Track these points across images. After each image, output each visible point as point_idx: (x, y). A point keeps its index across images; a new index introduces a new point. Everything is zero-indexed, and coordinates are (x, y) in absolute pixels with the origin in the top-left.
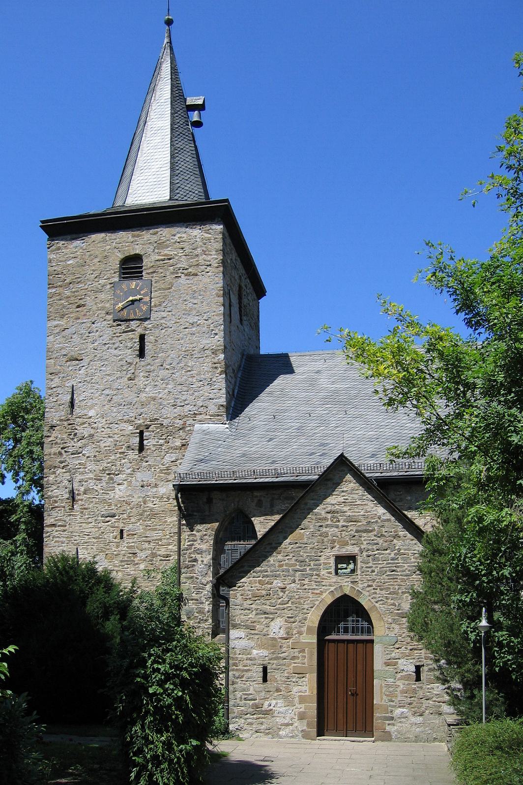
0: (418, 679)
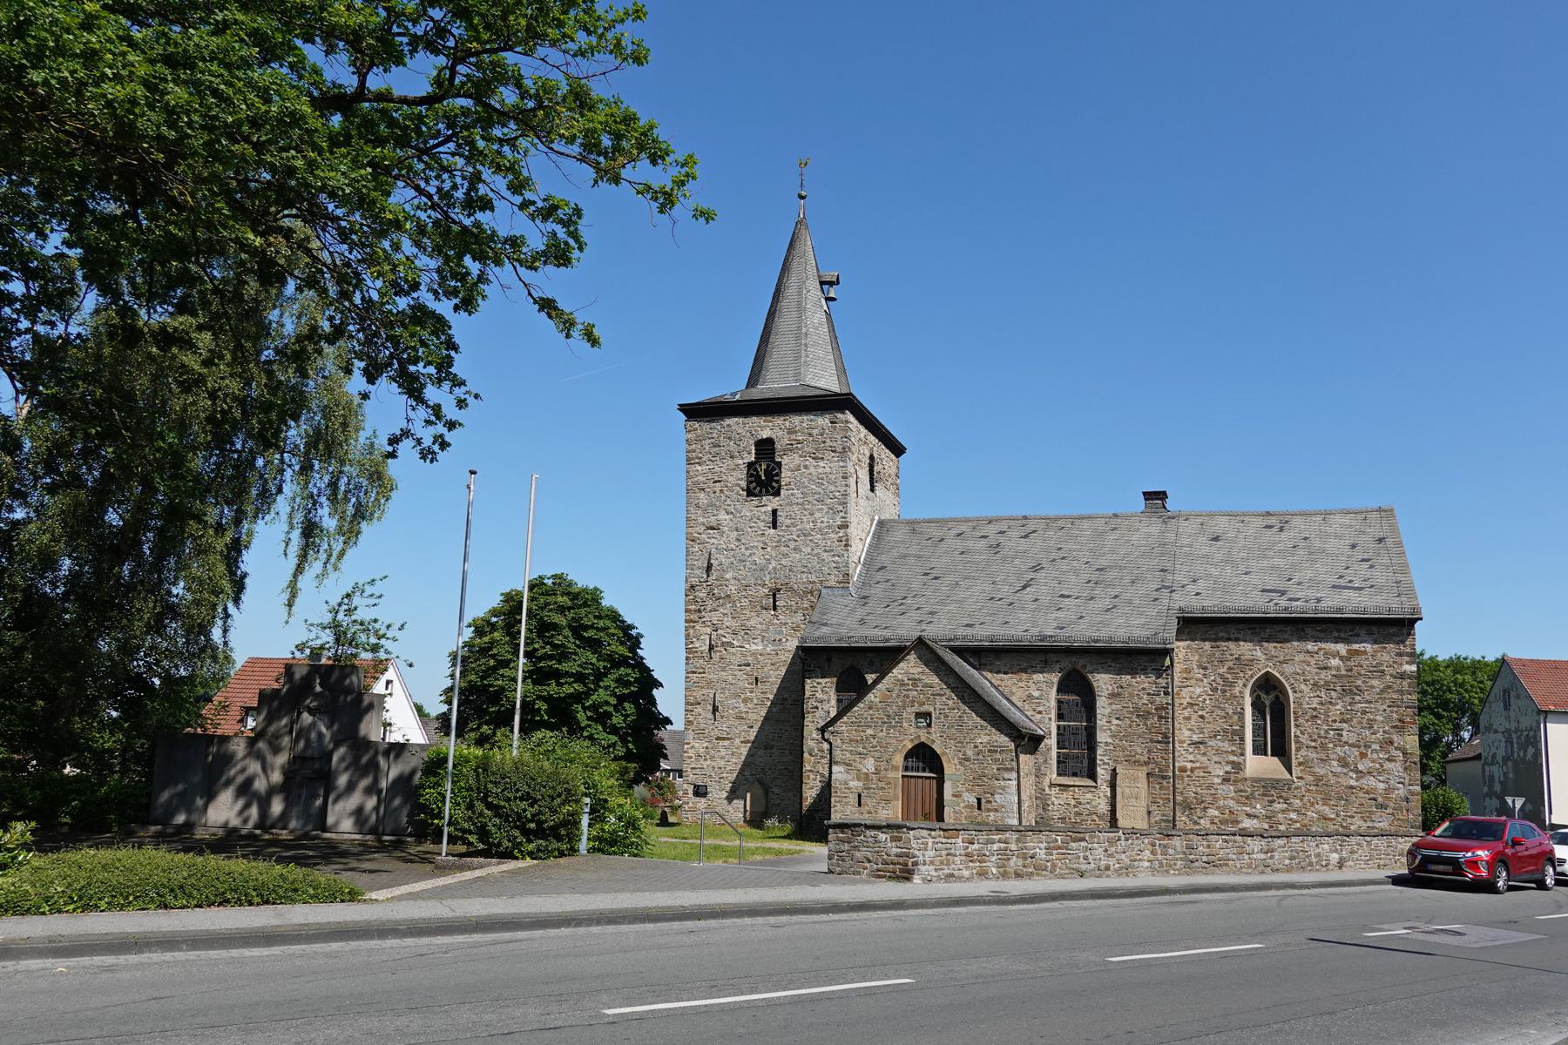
0: (979, 808)
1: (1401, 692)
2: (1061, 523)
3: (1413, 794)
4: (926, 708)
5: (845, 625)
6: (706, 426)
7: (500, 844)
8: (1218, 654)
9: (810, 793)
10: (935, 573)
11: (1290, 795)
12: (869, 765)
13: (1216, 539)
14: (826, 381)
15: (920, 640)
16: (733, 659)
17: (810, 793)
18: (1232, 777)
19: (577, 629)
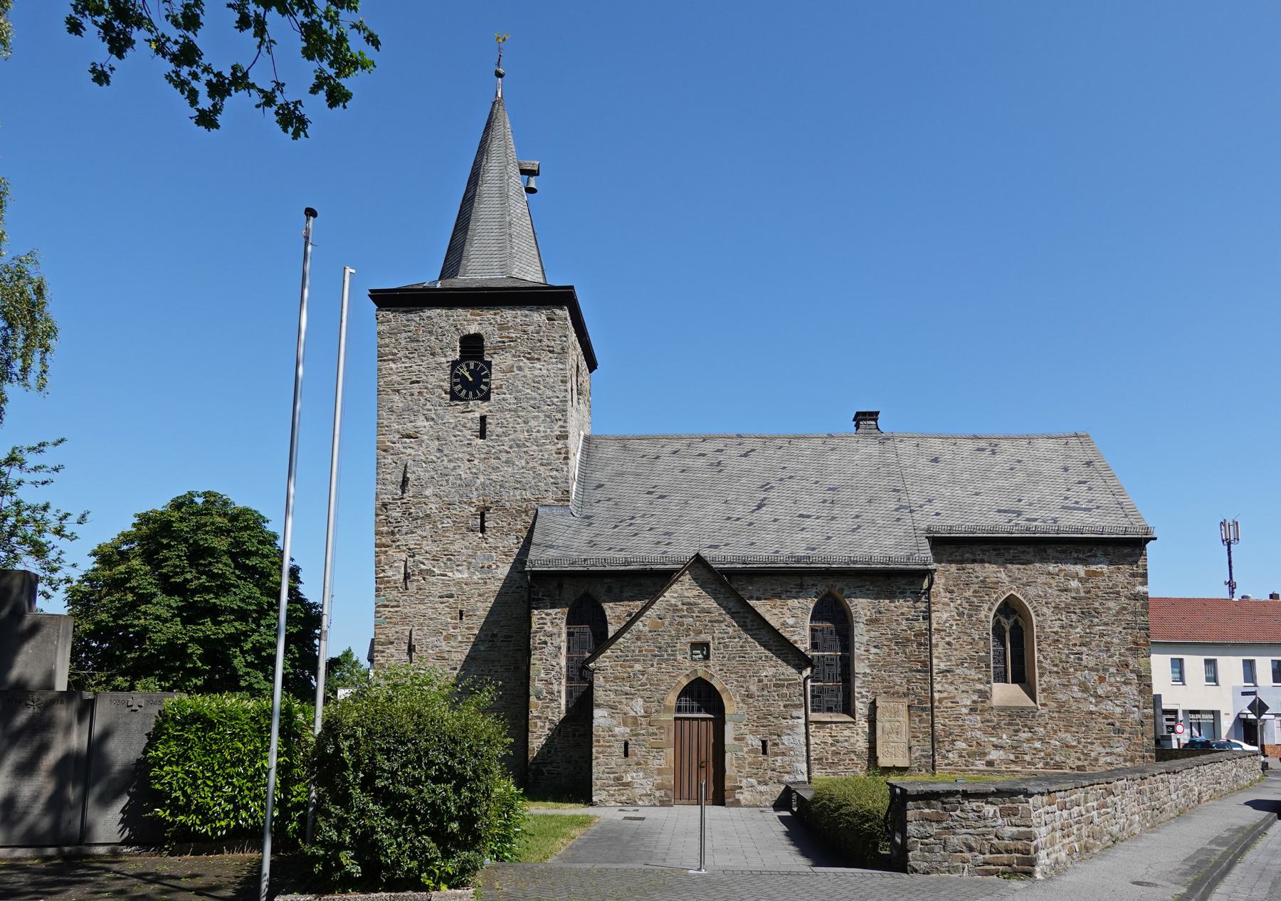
0: (765, 752)
1: (1134, 613)
2: (779, 442)
3: (1147, 717)
5: (564, 546)
6: (402, 318)
7: (397, 863)
8: (964, 577)
10: (659, 492)
11: (1035, 723)
12: (638, 706)
13: (936, 460)
14: (530, 274)
15: (698, 559)
16: (433, 589)
18: (979, 706)
19: (238, 554)
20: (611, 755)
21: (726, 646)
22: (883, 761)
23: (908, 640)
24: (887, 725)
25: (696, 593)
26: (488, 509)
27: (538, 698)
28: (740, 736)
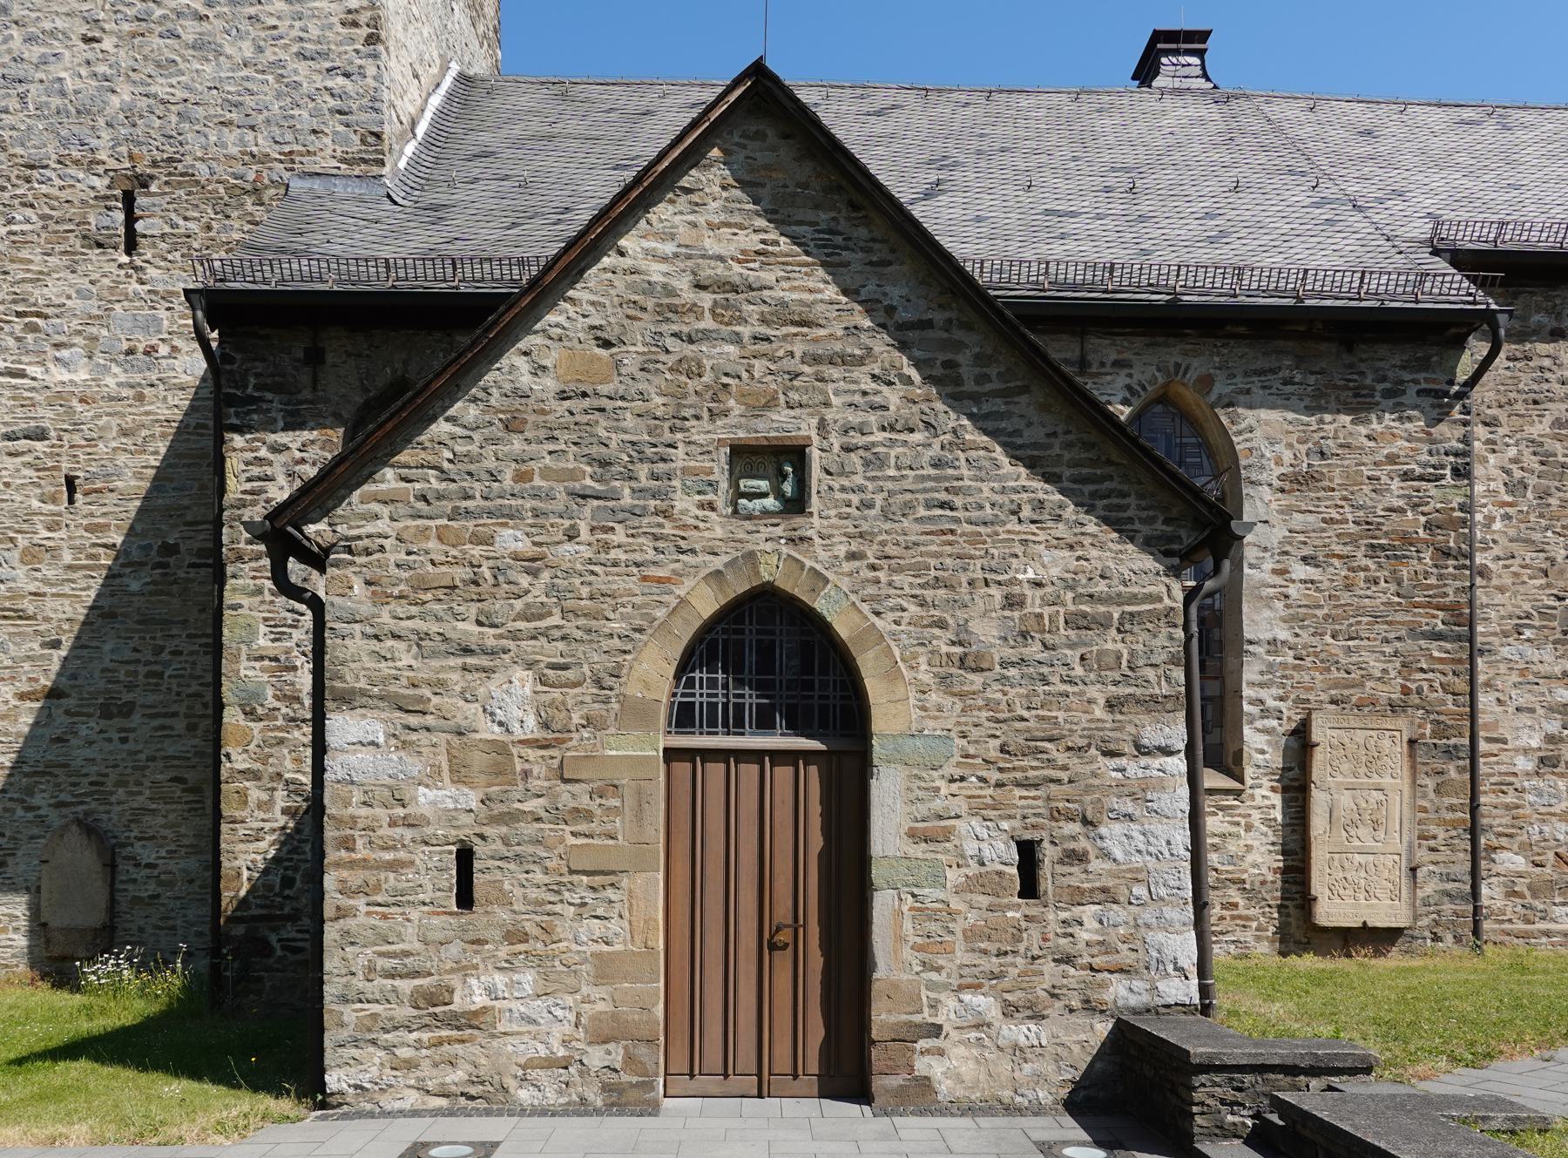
0: (1029, 888)
4: (780, 424)
9: (246, 855)
12: (514, 700)
17: (246, 855)
20: (399, 899)
21: (875, 461)
22: (1332, 911)
23: (1407, 539)
24: (1345, 800)
25: (752, 241)
26: (144, 182)
27: (250, 714)
28: (929, 823)
